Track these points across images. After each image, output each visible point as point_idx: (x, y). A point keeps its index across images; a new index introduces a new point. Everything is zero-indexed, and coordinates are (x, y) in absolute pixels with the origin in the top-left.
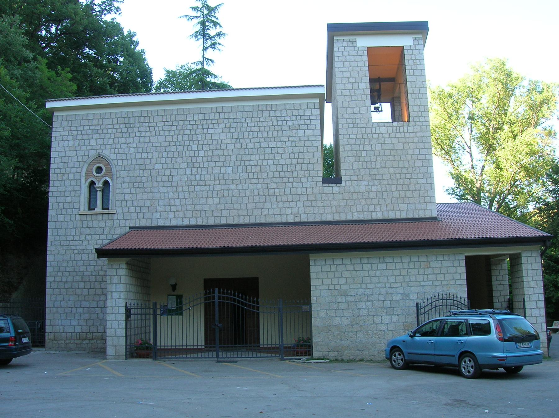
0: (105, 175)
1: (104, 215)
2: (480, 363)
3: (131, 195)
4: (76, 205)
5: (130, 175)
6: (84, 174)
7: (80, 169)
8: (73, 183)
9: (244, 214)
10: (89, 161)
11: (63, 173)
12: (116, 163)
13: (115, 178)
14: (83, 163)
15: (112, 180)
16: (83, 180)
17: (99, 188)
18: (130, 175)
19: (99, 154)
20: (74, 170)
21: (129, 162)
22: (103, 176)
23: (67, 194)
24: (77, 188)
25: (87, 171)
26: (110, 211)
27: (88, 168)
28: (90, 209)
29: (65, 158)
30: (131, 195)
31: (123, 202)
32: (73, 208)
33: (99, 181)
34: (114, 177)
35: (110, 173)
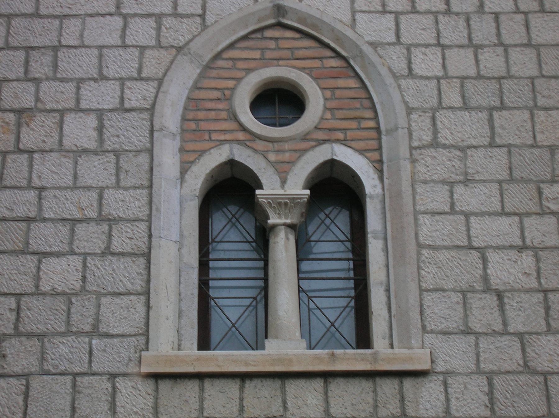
0: (324, 134)
1: (338, 388)
2: (348, 212)
3: (527, 259)
4: (120, 316)
5: (505, 137)
6: (170, 116)
7: (150, 88)
8: (96, 171)
9: (120, 194)
10: (206, 47)
11: (19, 112)
12: (401, 66)
13: (404, 151)
14: (166, 56)
15: (378, 165)
16: (168, 157)
17: (283, 205)
18: (505, 137)
19: (280, 10)
20: (102, 96)
21: (492, 62)
22: (310, 140)
23: (45, 236)
24: (122, 203)
25: (193, 103)
26: (384, 352)
27: (196, 87)
28: (204, 343)
29: (37, 24)
30: (527, 259)
31: (475, 301)
32: (95, 331)
33: (283, 172)
34: (395, 146)
35: (360, 113)
